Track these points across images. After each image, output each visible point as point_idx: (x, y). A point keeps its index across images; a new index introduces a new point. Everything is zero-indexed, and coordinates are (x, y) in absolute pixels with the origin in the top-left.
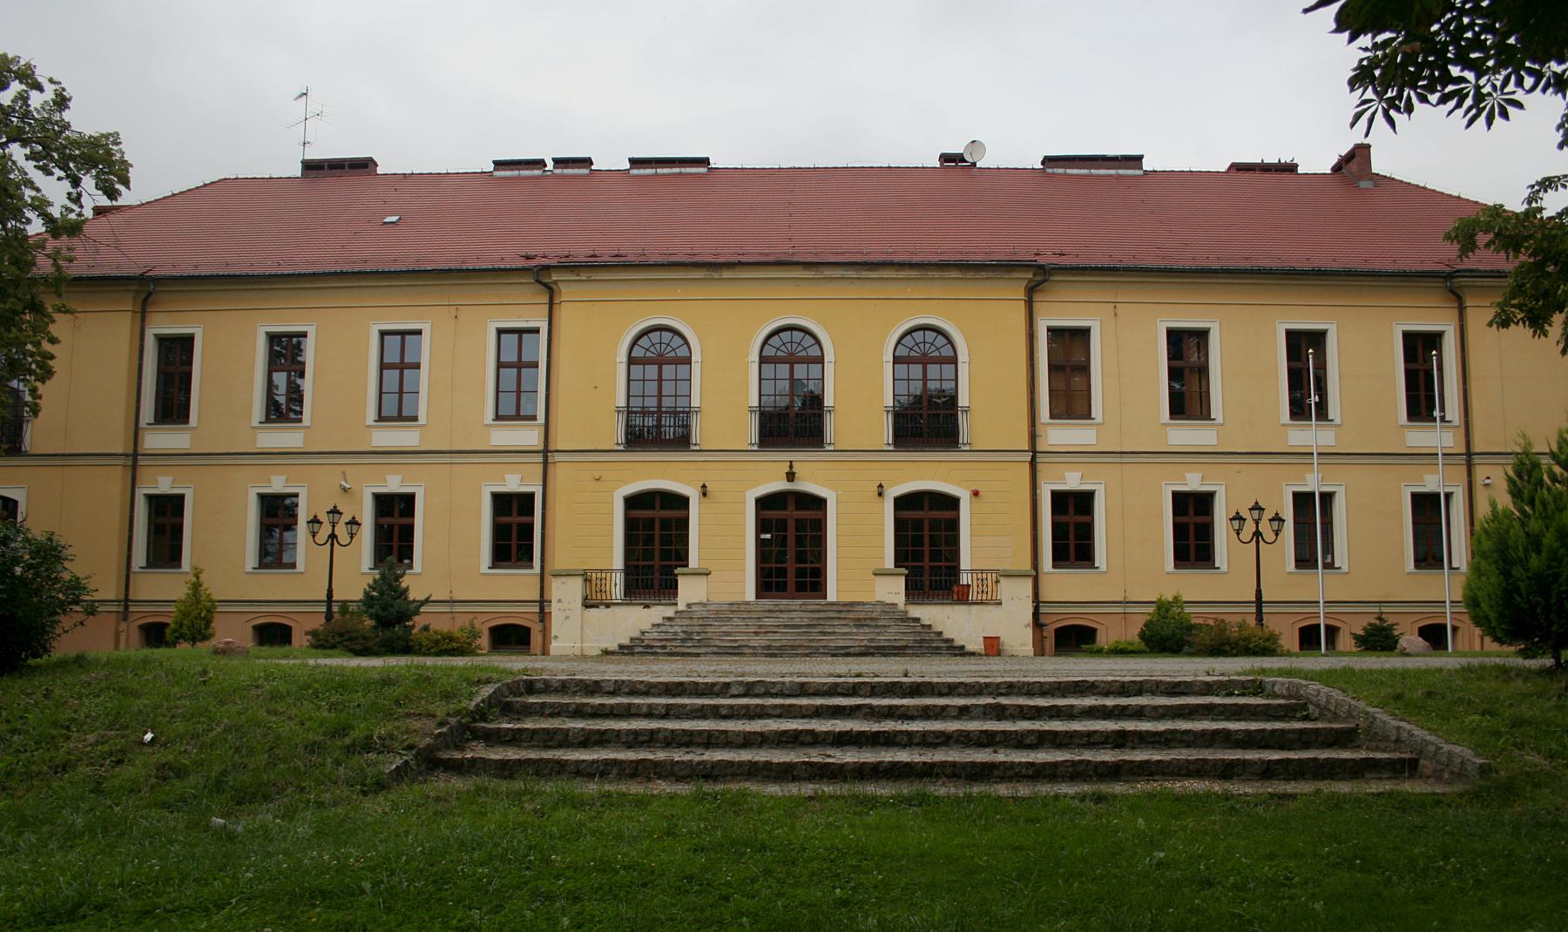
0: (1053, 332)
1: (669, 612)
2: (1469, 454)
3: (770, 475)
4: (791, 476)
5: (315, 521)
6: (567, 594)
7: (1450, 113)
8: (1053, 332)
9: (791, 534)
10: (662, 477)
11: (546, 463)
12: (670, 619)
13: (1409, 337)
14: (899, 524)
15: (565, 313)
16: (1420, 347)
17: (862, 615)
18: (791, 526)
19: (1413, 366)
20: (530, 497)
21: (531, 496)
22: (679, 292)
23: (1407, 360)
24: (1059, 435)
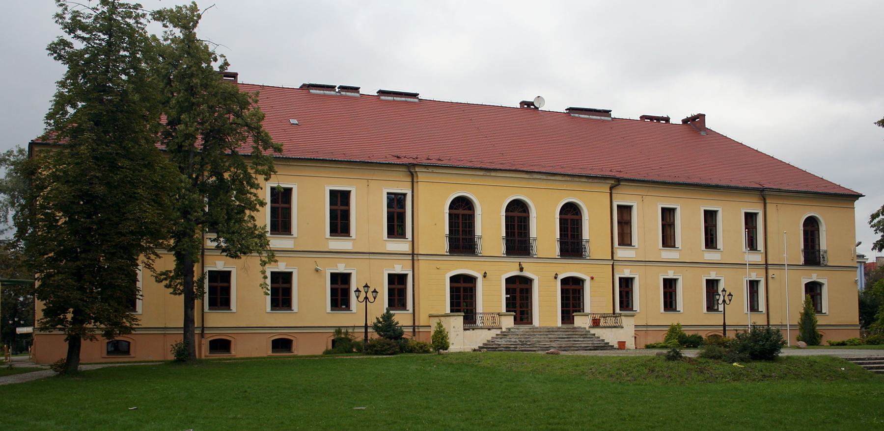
0: (619, 206)
2: (766, 264)
4: (521, 269)
5: (358, 291)
8: (619, 206)
9: (518, 295)
10: (471, 269)
11: (413, 260)
13: (663, 209)
14: (563, 291)
15: (421, 188)
16: (750, 218)
18: (518, 291)
19: (334, 207)
21: (406, 275)
22: (471, 180)
23: (388, 207)
24: (622, 253)
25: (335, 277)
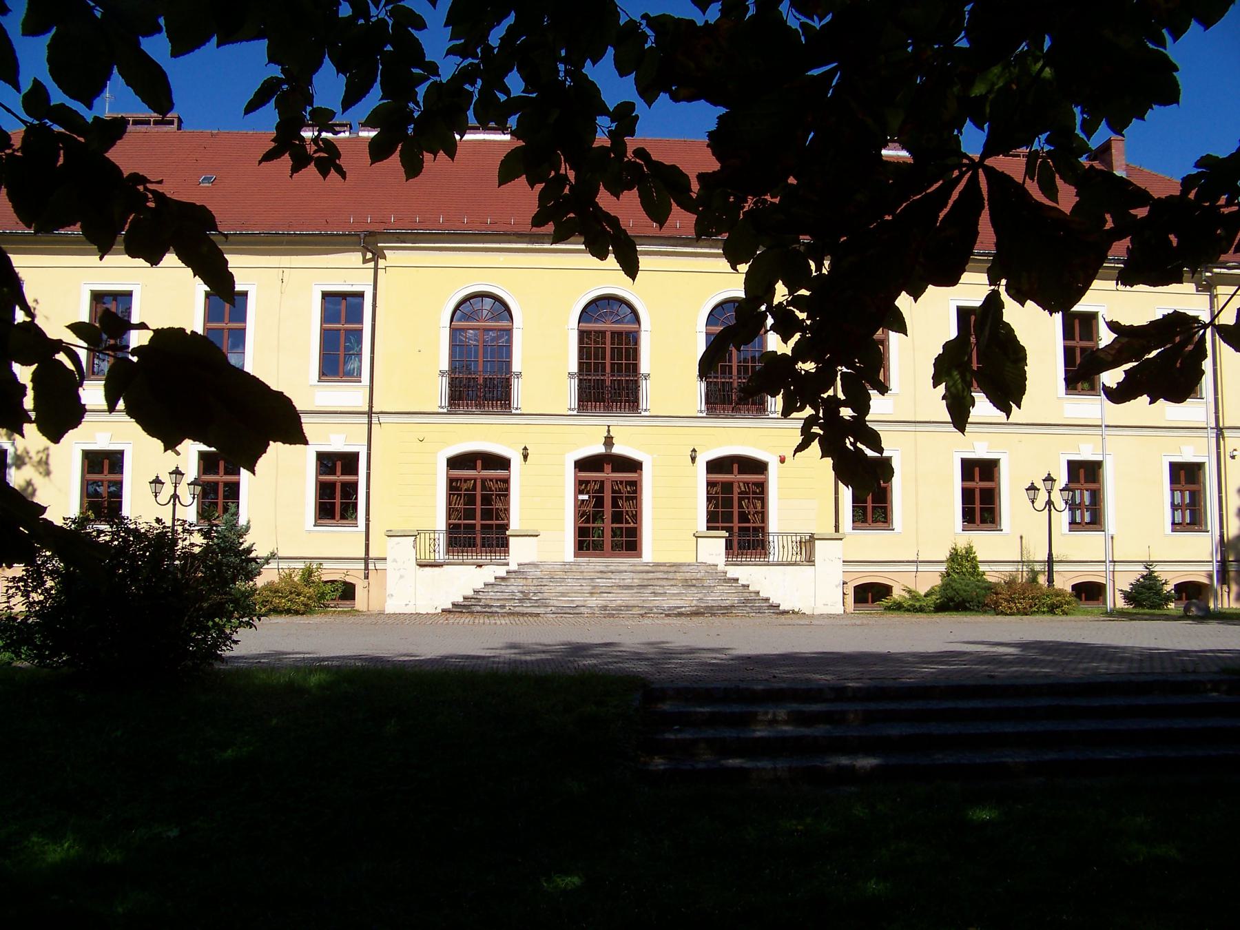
1: (501, 571)
3: (588, 437)
4: (609, 441)
6: (399, 557)
7: (160, 182)
12: (503, 579)
17: (688, 576)
20: (354, 457)
25: (969, 467)
